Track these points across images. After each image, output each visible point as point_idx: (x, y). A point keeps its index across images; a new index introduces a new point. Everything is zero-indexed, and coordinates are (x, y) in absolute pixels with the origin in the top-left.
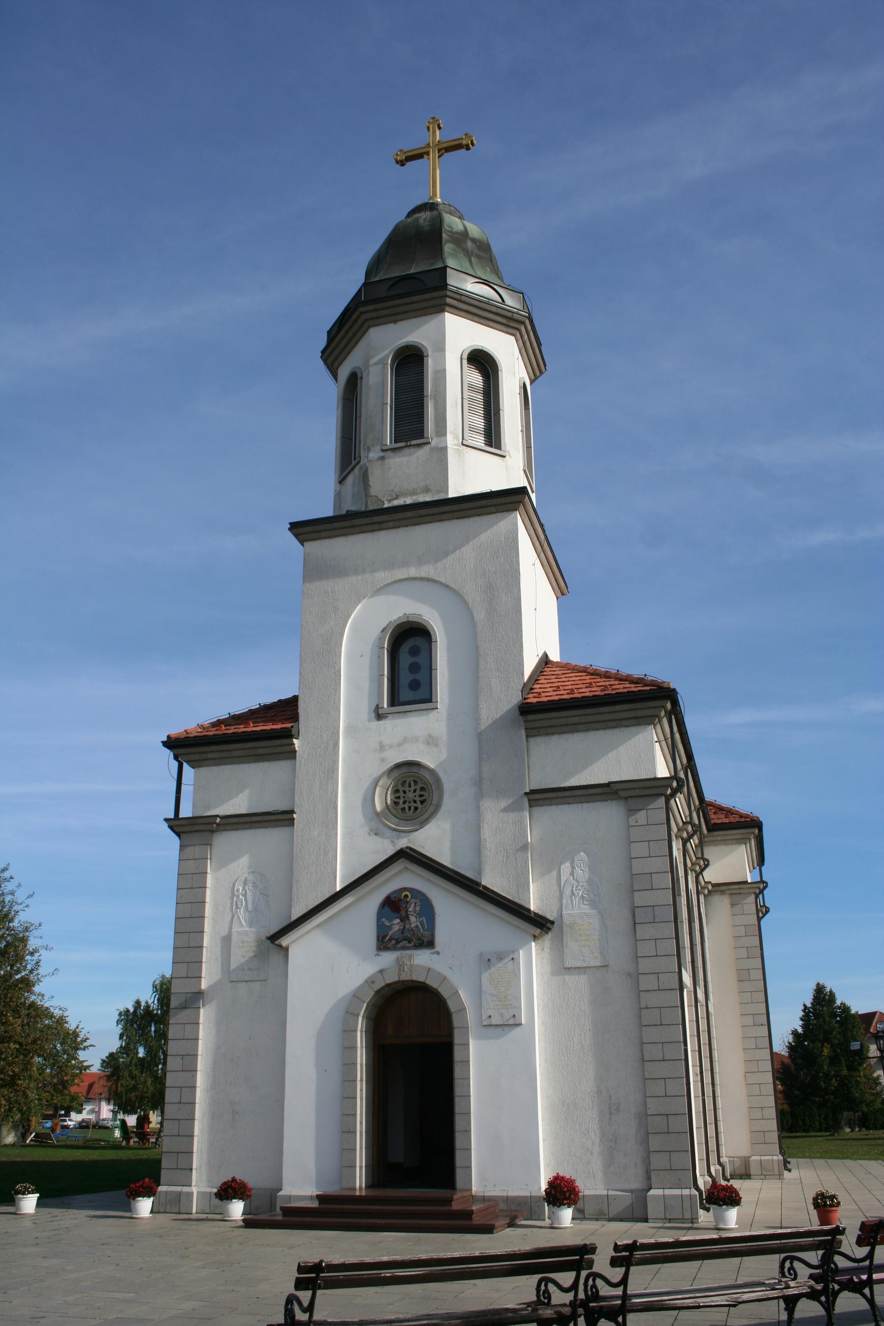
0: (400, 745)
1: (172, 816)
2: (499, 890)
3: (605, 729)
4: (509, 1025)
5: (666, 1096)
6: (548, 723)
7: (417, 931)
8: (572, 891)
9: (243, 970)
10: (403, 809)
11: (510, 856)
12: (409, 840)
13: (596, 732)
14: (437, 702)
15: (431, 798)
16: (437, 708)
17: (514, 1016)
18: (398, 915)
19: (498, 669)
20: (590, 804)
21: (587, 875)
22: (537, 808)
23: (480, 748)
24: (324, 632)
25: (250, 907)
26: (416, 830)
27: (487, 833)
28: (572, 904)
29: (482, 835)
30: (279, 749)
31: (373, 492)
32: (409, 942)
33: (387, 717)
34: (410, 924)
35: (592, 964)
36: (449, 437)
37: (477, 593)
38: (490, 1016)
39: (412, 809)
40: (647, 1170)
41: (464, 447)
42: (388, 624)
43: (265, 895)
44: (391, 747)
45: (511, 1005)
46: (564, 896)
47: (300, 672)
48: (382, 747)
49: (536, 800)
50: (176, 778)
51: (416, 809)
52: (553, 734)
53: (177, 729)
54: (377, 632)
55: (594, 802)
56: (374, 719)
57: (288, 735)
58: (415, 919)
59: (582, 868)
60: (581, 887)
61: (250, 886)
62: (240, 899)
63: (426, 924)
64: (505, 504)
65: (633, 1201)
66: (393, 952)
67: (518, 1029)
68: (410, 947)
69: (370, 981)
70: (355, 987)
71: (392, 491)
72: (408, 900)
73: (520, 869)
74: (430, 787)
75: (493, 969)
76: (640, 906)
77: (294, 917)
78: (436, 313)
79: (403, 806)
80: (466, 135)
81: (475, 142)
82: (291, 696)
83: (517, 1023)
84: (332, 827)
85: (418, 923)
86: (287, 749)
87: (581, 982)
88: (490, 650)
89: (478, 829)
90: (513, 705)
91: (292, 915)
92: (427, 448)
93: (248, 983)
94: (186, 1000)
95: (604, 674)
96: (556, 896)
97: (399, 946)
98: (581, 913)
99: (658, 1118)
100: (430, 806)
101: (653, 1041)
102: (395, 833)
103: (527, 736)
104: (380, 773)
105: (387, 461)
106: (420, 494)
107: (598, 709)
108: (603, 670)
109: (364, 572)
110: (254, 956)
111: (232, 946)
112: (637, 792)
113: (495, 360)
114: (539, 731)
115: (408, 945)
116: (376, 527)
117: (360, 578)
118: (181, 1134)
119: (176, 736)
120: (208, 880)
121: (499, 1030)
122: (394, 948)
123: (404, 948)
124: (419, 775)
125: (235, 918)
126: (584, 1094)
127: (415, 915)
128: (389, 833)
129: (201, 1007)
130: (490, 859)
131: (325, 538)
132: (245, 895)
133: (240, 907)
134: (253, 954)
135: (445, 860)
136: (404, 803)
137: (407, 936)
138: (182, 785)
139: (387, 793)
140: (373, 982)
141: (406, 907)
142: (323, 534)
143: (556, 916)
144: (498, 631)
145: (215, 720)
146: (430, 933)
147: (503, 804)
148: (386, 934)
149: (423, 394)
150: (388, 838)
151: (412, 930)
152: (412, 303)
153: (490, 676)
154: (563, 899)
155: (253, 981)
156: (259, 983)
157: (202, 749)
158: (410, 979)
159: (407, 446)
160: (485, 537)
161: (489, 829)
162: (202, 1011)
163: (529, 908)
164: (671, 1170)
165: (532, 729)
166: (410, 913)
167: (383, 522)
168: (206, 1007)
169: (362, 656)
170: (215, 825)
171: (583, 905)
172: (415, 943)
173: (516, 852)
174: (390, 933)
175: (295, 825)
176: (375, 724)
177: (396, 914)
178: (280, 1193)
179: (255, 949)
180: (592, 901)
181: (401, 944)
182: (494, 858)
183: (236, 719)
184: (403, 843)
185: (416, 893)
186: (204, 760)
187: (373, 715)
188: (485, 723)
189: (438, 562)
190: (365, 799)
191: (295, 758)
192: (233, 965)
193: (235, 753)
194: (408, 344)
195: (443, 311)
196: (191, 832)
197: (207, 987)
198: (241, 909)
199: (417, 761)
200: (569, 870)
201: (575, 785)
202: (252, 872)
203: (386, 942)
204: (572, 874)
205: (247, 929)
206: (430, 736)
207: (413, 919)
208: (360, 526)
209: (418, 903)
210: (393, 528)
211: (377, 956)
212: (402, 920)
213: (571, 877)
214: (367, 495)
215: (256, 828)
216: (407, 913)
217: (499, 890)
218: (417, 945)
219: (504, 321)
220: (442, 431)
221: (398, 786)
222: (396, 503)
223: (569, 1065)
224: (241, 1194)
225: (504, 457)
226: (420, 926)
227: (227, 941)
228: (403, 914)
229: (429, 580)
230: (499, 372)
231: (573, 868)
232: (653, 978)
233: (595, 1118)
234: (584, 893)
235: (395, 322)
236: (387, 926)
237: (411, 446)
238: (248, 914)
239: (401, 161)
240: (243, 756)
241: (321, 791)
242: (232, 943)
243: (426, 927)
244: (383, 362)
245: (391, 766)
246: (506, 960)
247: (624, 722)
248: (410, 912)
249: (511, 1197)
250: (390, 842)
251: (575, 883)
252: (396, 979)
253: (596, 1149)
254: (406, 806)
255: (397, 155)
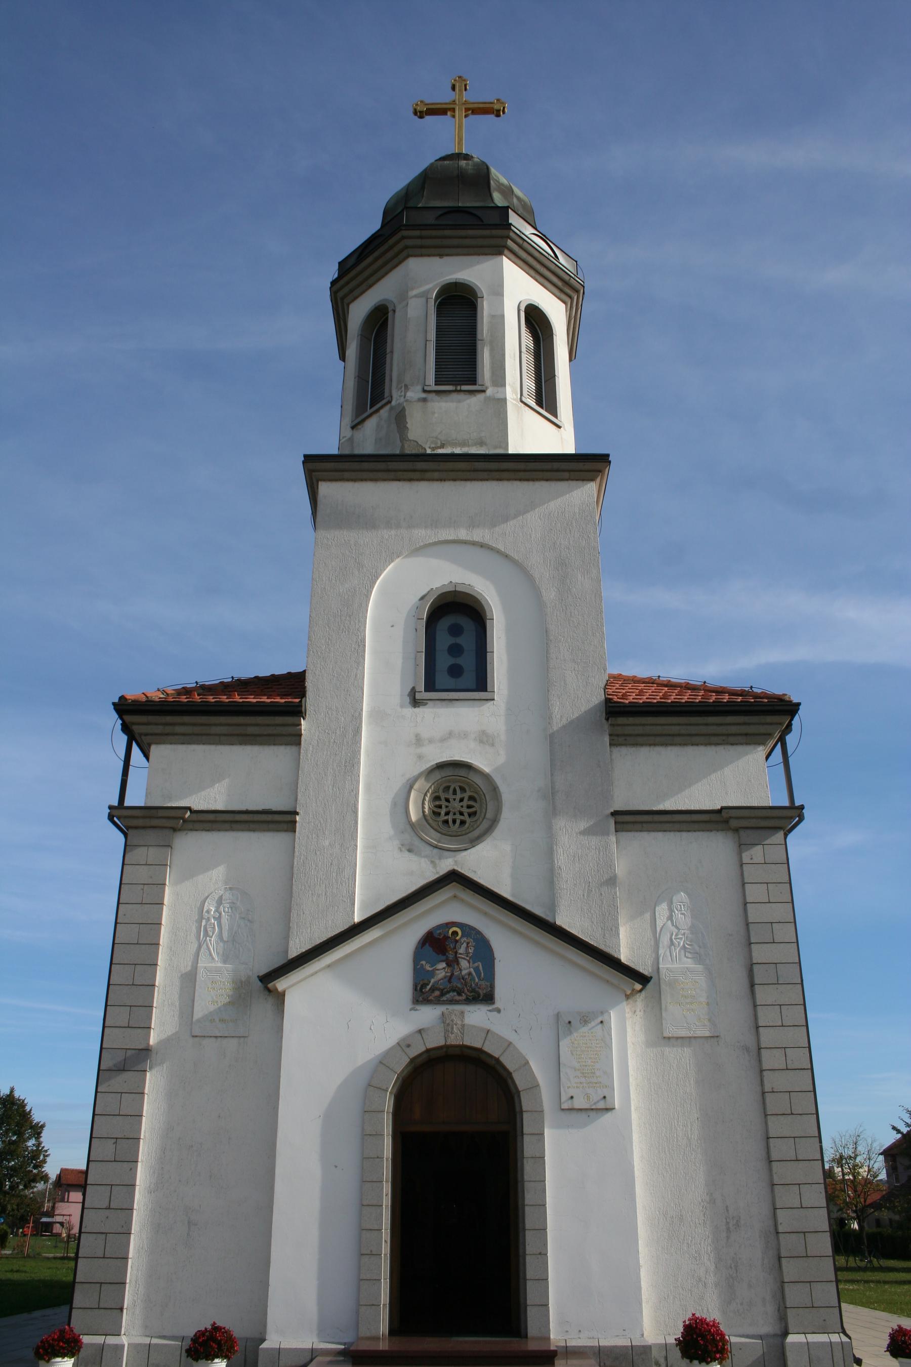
0: (443, 740)
1: (116, 803)
2: (579, 933)
3: (706, 744)
4: (597, 1109)
5: (802, 1207)
6: (639, 730)
7: (471, 980)
8: (671, 939)
9: (212, 1021)
10: (446, 822)
11: (593, 890)
12: (456, 862)
13: (695, 748)
14: (494, 692)
15: (484, 811)
16: (494, 700)
17: (605, 1097)
18: (444, 958)
19: (574, 660)
20: (690, 834)
21: (689, 921)
22: (624, 833)
23: (552, 752)
24: (343, 591)
25: (225, 935)
26: (466, 850)
27: (561, 859)
28: (671, 956)
29: (556, 862)
30: (279, 730)
31: (411, 435)
32: (459, 994)
33: (426, 704)
34: (461, 970)
35: (699, 1033)
36: (508, 389)
37: (546, 568)
38: (572, 1097)
39: (458, 822)
40: (779, 1308)
41: (523, 405)
42: (429, 592)
43: (249, 920)
44: (431, 741)
45: (600, 1082)
46: (661, 945)
47: (309, 637)
48: (418, 741)
49: (623, 823)
50: (123, 757)
51: (463, 823)
52: (642, 745)
53: (133, 692)
54: (414, 599)
55: (695, 831)
56: (409, 705)
57: (298, 712)
58: (468, 965)
59: (683, 912)
60: (682, 935)
61: (225, 908)
62: (211, 923)
63: (482, 972)
64: (581, 471)
65: (765, 1350)
66: (435, 1006)
67: (608, 1116)
68: (460, 1000)
69: (403, 1044)
70: (380, 1052)
71: (436, 438)
72: (458, 938)
73: (606, 907)
74: (483, 797)
75: (575, 1034)
76: (759, 962)
77: (293, 953)
78: (493, 254)
79: (446, 818)
80: (498, 100)
81: (506, 110)
82: (269, 675)
83: (608, 1107)
84: (350, 837)
85: (472, 970)
86: (291, 730)
87: (684, 1056)
88: (564, 637)
89: (550, 853)
90: (593, 704)
91: (289, 949)
92: (481, 396)
93: (219, 1039)
94: (125, 1060)
95: (686, 685)
96: (651, 945)
97: (444, 998)
98: (684, 968)
99: (793, 1236)
100: (483, 820)
101: (783, 1136)
102: (436, 851)
103: (611, 745)
104: (416, 773)
105: (429, 404)
106: (473, 446)
107: (706, 718)
108: (683, 681)
109: (398, 526)
110: (229, 1002)
111: (197, 987)
112: (752, 823)
113: (550, 322)
114: (626, 740)
115: (457, 998)
116: (417, 475)
117: (393, 532)
118: (107, 1255)
119: (133, 698)
120: (165, 895)
121: (583, 1115)
122: (438, 1001)
123: (452, 1002)
124: (468, 781)
125: (202, 949)
126: (692, 1205)
127: (468, 958)
128: (428, 850)
129: (148, 1070)
130: (567, 893)
131: (348, 480)
132: (219, 919)
133: (211, 934)
134: (228, 1000)
135: (505, 891)
136: (447, 814)
137: (457, 987)
138: (130, 767)
139: (424, 799)
140: (409, 1046)
141: (455, 948)
142: (346, 475)
143: (650, 970)
144: (573, 614)
145: (180, 687)
146: (488, 984)
147: (583, 825)
148: (426, 981)
149: (476, 337)
150: (426, 857)
151: (463, 978)
152: (466, 237)
153: (563, 666)
154: (660, 948)
155: (226, 1037)
156: (235, 1041)
157: (169, 719)
158: (461, 1043)
159: (456, 391)
160: (553, 505)
161: (565, 855)
162: (148, 1074)
163: (619, 957)
164: (813, 1307)
165: (618, 735)
166: (460, 956)
167: (426, 471)
168: (154, 1071)
169: (392, 626)
170: (181, 821)
171: (685, 959)
172: (467, 995)
173: (601, 886)
174: (432, 981)
175: (297, 830)
176: (410, 711)
177: (440, 955)
178: (264, 1345)
179: (231, 993)
180: (697, 953)
181: (448, 996)
182: (572, 892)
183: (205, 689)
184: (446, 865)
185: (468, 930)
186: (167, 734)
187: (407, 700)
188: (558, 722)
189: (495, 526)
190: (394, 804)
191: (299, 744)
192: (198, 1013)
193: (214, 730)
194: (457, 281)
195: (501, 253)
196: (144, 828)
197: (156, 1042)
198: (211, 937)
199: (467, 762)
200: (666, 913)
201: (671, 809)
202: (231, 889)
203: (426, 992)
204: (670, 918)
205: (220, 965)
206: (484, 732)
207: (464, 964)
208: (395, 471)
209: (472, 943)
210: (437, 480)
211: (413, 1012)
212: (448, 965)
213: (669, 922)
214: (403, 437)
215: (238, 830)
216: (456, 955)
217: (579, 933)
218: (471, 998)
219: (559, 283)
220: (500, 380)
221: (439, 792)
222: (440, 451)
223: (672, 1164)
224: (228, 1350)
225: (559, 427)
226: (474, 974)
227: (189, 980)
228: (451, 956)
229: (482, 546)
230: (554, 336)
231: (671, 911)
232: (779, 1053)
233: (709, 1237)
234: (687, 944)
235: (441, 256)
236: (428, 971)
237: (461, 391)
238: (221, 944)
239: (420, 112)
240: (225, 735)
241: (334, 789)
242: (197, 983)
243: (482, 974)
244: (425, 295)
245: (433, 765)
246: (593, 1024)
247: (731, 739)
248: (460, 954)
249: (605, 1347)
250: (429, 863)
251: (675, 930)
252: (441, 1042)
253: (711, 1279)
254: (450, 818)
255: (417, 105)
